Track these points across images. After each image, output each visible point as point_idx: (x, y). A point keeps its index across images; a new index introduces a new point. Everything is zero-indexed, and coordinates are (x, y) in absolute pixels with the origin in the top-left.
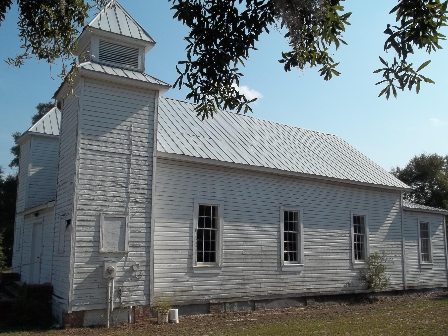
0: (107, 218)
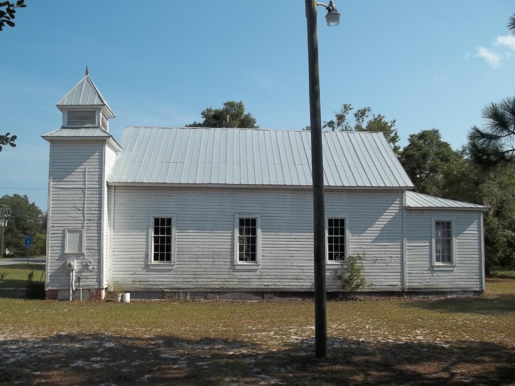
0: (70, 231)
